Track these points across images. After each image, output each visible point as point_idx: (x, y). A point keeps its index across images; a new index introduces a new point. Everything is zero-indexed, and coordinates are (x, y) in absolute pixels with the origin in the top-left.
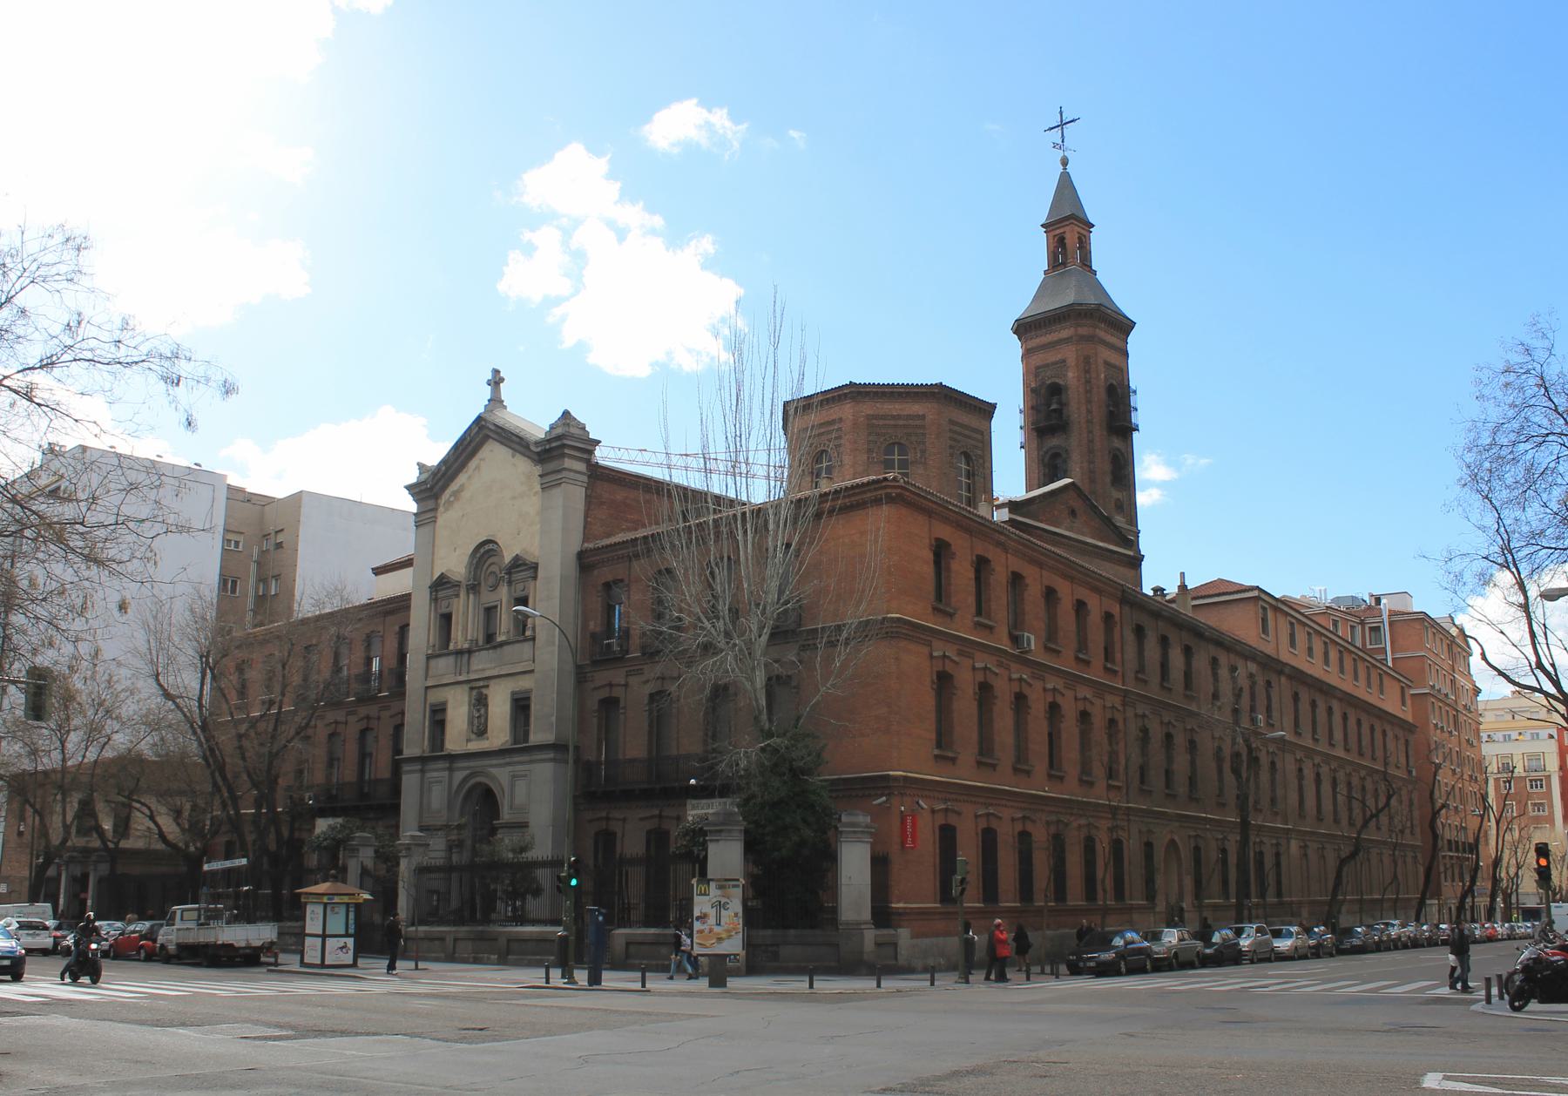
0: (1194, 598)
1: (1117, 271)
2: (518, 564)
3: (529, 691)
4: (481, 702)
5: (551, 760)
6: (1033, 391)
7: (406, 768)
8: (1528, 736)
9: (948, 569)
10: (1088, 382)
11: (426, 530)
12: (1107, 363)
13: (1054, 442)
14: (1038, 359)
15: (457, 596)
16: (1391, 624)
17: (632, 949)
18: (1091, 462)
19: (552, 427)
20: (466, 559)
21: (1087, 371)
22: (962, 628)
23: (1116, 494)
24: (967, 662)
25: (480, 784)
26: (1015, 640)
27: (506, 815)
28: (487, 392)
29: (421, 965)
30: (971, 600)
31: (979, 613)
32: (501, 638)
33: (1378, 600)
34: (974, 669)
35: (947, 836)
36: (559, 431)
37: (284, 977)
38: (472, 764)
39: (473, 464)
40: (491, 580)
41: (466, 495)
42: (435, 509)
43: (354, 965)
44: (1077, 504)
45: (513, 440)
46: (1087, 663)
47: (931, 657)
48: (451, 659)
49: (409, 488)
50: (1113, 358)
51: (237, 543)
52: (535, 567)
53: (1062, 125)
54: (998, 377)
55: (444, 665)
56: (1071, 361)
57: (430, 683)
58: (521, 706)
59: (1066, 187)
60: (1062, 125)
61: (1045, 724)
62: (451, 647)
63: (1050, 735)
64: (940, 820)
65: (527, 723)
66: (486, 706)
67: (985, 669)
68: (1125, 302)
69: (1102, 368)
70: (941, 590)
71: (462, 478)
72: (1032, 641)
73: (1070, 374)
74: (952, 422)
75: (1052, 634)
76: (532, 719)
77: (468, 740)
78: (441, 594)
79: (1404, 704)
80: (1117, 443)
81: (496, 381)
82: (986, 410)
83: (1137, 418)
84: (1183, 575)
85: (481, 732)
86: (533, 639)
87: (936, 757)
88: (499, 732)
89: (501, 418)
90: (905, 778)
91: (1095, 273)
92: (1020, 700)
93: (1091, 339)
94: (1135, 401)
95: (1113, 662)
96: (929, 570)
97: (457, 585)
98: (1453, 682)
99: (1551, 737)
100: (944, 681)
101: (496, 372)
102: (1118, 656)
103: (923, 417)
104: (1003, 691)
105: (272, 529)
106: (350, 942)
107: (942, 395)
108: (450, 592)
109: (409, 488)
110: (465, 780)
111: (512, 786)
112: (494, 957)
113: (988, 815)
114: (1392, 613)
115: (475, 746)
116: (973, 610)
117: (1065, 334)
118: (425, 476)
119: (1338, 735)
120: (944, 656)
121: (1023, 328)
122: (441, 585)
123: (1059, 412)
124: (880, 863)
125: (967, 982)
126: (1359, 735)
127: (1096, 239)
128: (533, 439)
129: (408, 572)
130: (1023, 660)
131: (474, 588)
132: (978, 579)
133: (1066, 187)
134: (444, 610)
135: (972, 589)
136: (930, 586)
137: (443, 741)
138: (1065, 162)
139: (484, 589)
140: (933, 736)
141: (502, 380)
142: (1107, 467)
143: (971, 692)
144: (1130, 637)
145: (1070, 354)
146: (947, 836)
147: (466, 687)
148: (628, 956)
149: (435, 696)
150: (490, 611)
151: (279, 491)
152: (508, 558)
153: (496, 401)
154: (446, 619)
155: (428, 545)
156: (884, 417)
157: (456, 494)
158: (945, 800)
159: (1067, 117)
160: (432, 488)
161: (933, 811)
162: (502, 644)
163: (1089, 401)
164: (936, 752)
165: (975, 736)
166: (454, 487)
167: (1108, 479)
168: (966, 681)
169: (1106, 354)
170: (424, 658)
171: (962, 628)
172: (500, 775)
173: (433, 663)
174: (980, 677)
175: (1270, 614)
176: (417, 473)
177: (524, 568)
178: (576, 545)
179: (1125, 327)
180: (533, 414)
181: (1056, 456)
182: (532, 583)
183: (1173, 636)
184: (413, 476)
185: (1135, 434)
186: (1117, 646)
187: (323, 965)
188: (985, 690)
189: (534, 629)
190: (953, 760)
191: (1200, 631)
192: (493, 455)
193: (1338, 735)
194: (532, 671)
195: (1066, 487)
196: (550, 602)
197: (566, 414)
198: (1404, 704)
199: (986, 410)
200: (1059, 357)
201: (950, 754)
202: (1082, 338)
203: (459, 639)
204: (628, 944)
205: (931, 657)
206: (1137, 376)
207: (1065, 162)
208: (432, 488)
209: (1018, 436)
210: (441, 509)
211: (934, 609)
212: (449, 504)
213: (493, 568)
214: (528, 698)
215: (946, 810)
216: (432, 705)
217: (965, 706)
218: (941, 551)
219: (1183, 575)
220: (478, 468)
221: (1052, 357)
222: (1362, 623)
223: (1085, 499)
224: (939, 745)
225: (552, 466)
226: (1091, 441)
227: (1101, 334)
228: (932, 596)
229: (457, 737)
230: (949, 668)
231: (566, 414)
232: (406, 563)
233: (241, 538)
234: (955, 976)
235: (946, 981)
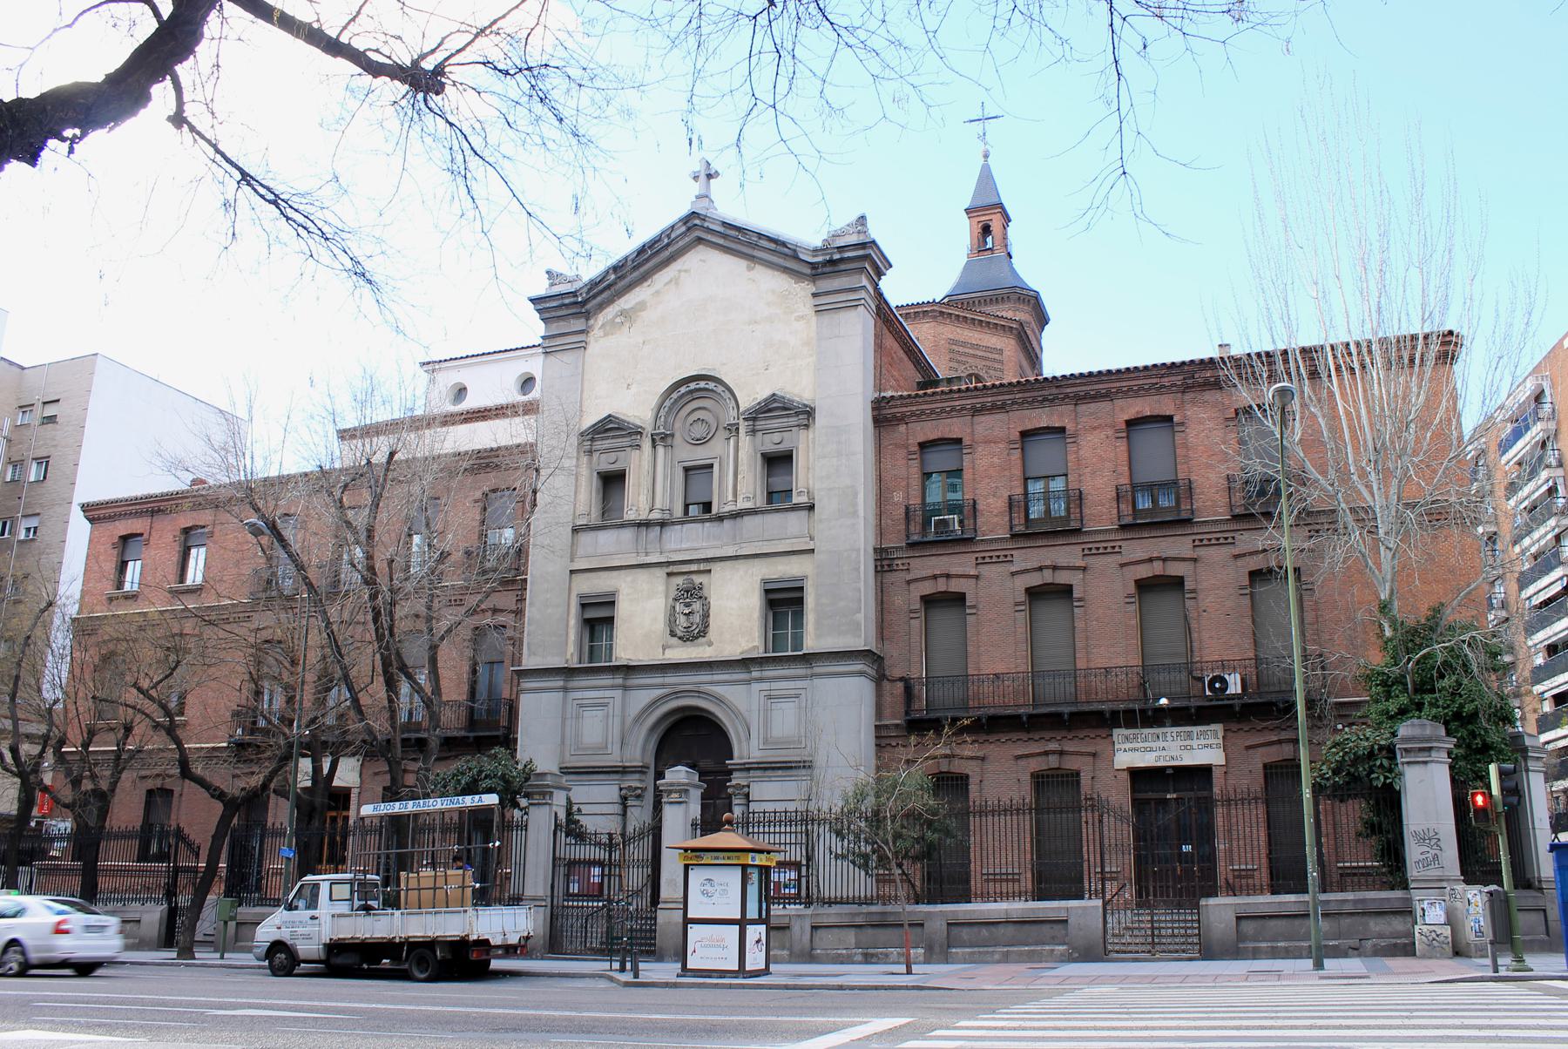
2: (774, 408)
5: (861, 673)
7: (527, 684)
20: (654, 401)
38: (668, 680)
39: (662, 277)
48: (627, 534)
55: (612, 544)
58: (783, 602)
59: (986, 179)
78: (598, 445)
103: (1001, 352)
108: (626, 441)
133: (986, 179)
138: (986, 156)
147: (660, 573)
148: (1241, 937)
156: (964, 344)
160: (584, 303)
176: (547, 283)
178: (872, 395)
182: (803, 433)
196: (840, 465)
203: (636, 501)
207: (986, 156)
210: (596, 332)
220: (675, 281)
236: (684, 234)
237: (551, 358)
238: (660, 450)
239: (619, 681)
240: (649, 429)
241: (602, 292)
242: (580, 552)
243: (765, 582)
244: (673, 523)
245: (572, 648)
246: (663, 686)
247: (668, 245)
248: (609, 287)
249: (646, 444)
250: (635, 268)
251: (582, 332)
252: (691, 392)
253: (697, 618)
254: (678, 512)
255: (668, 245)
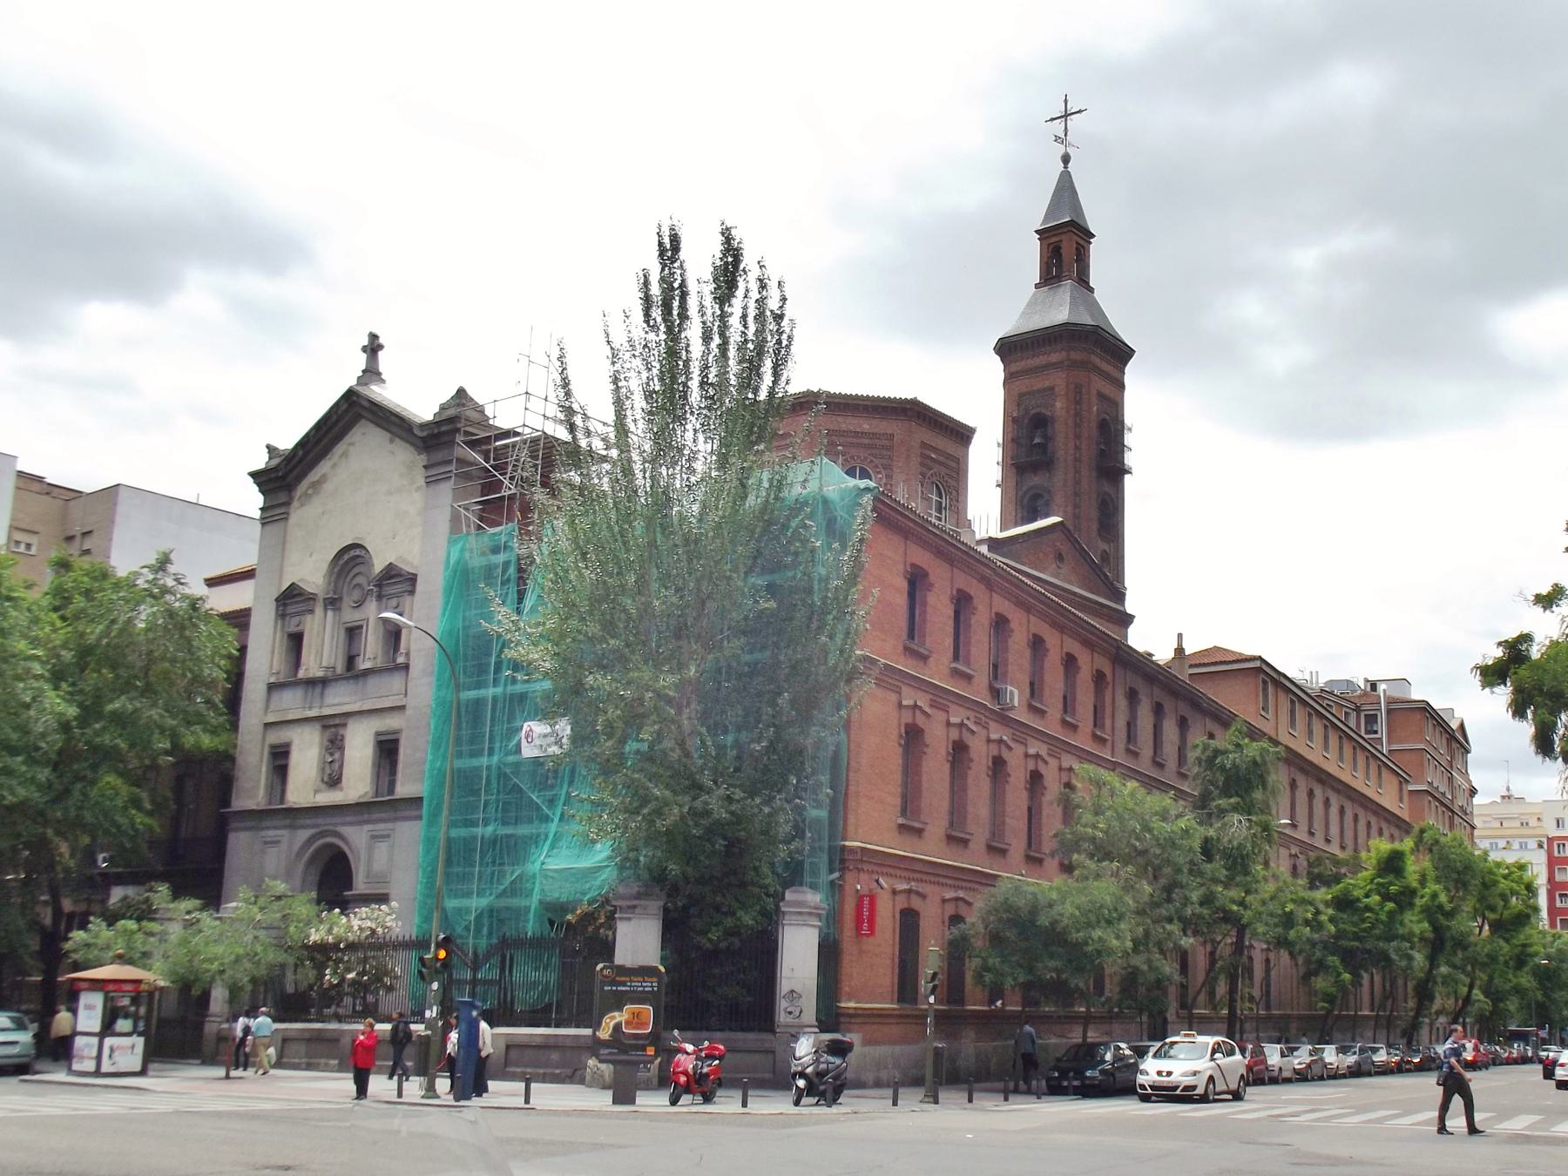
0: (1191, 666)
1: (1118, 289)
3: (397, 732)
4: (335, 745)
6: (1015, 420)
8: (1516, 846)
9: (924, 604)
10: (1077, 414)
11: (274, 529)
12: (1101, 395)
13: (1035, 480)
14: (1023, 385)
15: (312, 611)
16: (1389, 711)
17: (513, 1054)
18: (1076, 506)
19: (443, 408)
20: (324, 566)
21: (1078, 403)
22: (937, 673)
23: (1103, 546)
24: (940, 716)
25: (331, 845)
26: (996, 694)
27: (360, 885)
28: (361, 361)
29: (233, 1073)
30: (949, 642)
31: (956, 657)
32: (363, 664)
33: (1374, 686)
34: (948, 724)
35: (909, 921)
36: (451, 412)
37: (40, 1086)
38: (320, 821)
40: (356, 595)
41: (328, 487)
42: (288, 504)
43: (143, 1072)
44: (1065, 548)
45: (392, 422)
46: (1074, 728)
47: (900, 706)
49: (254, 475)
50: (1108, 389)
51: (28, 546)
52: (413, 579)
53: (1066, 115)
54: (975, 395)
55: (291, 703)
56: (1061, 388)
57: (271, 719)
58: (387, 749)
59: (1066, 190)
60: (1066, 115)
61: (1025, 794)
62: (301, 674)
63: (1030, 809)
64: (901, 902)
65: (393, 771)
66: (341, 749)
67: (961, 725)
68: (1123, 327)
69: (1094, 400)
70: (913, 629)
71: (324, 467)
72: (1015, 695)
73: (1058, 405)
74: (924, 445)
75: (1035, 689)
76: (400, 766)
77: (316, 792)
78: (290, 610)
79: (1401, 800)
80: (1107, 488)
81: (373, 347)
82: (962, 434)
83: (1130, 459)
84: (1180, 636)
85: (334, 781)
86: (406, 667)
87: (901, 826)
88: (358, 783)
89: (377, 392)
90: (863, 849)
91: (1091, 290)
92: (998, 764)
93: (1084, 365)
94: (1128, 439)
95: (1103, 727)
96: (901, 600)
97: (312, 598)
98: (1451, 779)
99: (1540, 846)
100: (913, 737)
101: (373, 337)
102: (1108, 722)
104: (980, 752)
105: (77, 530)
106: (139, 1042)
107: (914, 412)
109: (254, 475)
110: (310, 841)
111: (370, 849)
112: (335, 1062)
113: (957, 899)
114: (1391, 701)
115: (327, 798)
116: (950, 654)
117: (1055, 357)
118: (275, 462)
119: (1334, 830)
120: (915, 706)
121: (1008, 348)
122: (291, 599)
123: (1042, 447)
124: (829, 954)
125: (936, 1102)
126: (1356, 831)
127: (1095, 248)
128: (418, 421)
129: (247, 587)
130: (1004, 719)
131: (333, 603)
132: (957, 613)
133: (1066, 190)
134: (293, 629)
135: (950, 628)
136: (903, 623)
137: (283, 792)
138: (1066, 159)
139: (347, 602)
140: (898, 801)
141: (381, 347)
142: (1094, 514)
143: (943, 752)
144: (1122, 703)
145: (1058, 380)
146: (909, 921)
148: (506, 1063)
149: (276, 737)
150: (353, 633)
151: (88, 480)
152: (378, 566)
153: (372, 373)
154: (296, 640)
155: (275, 549)
157: (316, 485)
158: (909, 880)
159: (1072, 107)
160: (284, 478)
161: (894, 892)
162: (367, 673)
163: (1078, 437)
164: (900, 821)
165: (946, 805)
166: (314, 476)
167: (1095, 526)
168: (938, 738)
169: (1099, 384)
170: (264, 688)
171: (937, 673)
172: (356, 837)
173: (276, 696)
174: (954, 734)
175: (1270, 689)
176: (266, 457)
177: (397, 582)
179: (1122, 354)
180: (416, 394)
181: (1037, 497)
183: (1168, 705)
184: (261, 461)
185: (1127, 477)
186: (1108, 711)
187: (97, 1073)
188: (959, 751)
189: (408, 654)
190: (919, 832)
191: (1202, 696)
192: (365, 444)
193: (1334, 830)
194: (402, 708)
195: (1054, 525)
197: (461, 392)
198: (1401, 800)
199: (962, 434)
200: (1047, 384)
201: (916, 825)
202: (1074, 365)
203: (312, 666)
204: (508, 1047)
205: (900, 706)
206: (1130, 416)
207: (1066, 159)
208: (283, 479)
209: (996, 473)
210: (295, 504)
211: (906, 649)
212: (307, 497)
213: (359, 580)
214: (396, 742)
215: (909, 891)
216: (273, 747)
217: (936, 768)
218: (916, 581)
219: (1180, 636)
220: (345, 454)
221: (1039, 383)
222: (1358, 710)
223: (1075, 543)
224: (904, 813)
225: (440, 455)
226: (1077, 483)
227: (1097, 361)
228: (904, 636)
229: (303, 787)
230: (920, 720)
231: (461, 392)
232: (248, 574)
233: (33, 540)
234: (920, 1093)
235: (911, 1098)
236: (346, 411)
237: (268, 528)
238: (330, 613)
239: (288, 822)
240: (321, 595)
241: (295, 467)
242: (272, 707)
243: (378, 734)
244: (336, 680)
245: (261, 792)
246: (313, 826)
247: (338, 421)
248: (300, 461)
249: (319, 610)
250: (317, 443)
251: (283, 504)
252: (347, 563)
253: (336, 766)
254: (340, 669)
255: (338, 421)
